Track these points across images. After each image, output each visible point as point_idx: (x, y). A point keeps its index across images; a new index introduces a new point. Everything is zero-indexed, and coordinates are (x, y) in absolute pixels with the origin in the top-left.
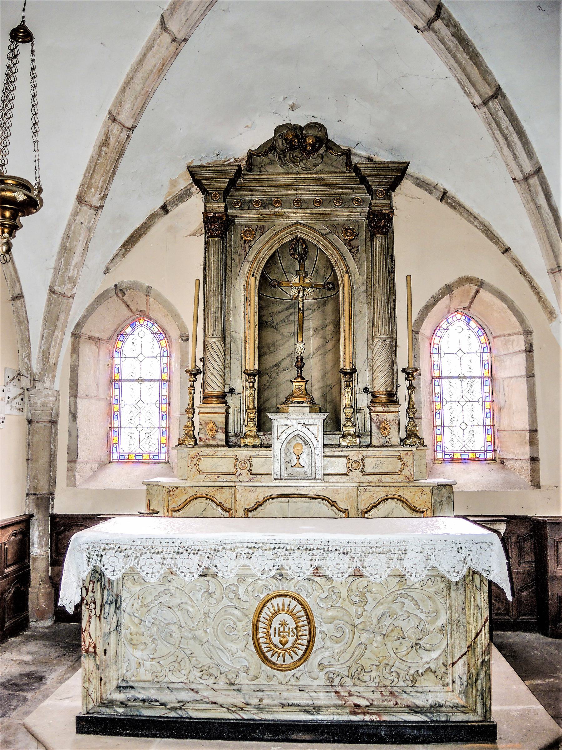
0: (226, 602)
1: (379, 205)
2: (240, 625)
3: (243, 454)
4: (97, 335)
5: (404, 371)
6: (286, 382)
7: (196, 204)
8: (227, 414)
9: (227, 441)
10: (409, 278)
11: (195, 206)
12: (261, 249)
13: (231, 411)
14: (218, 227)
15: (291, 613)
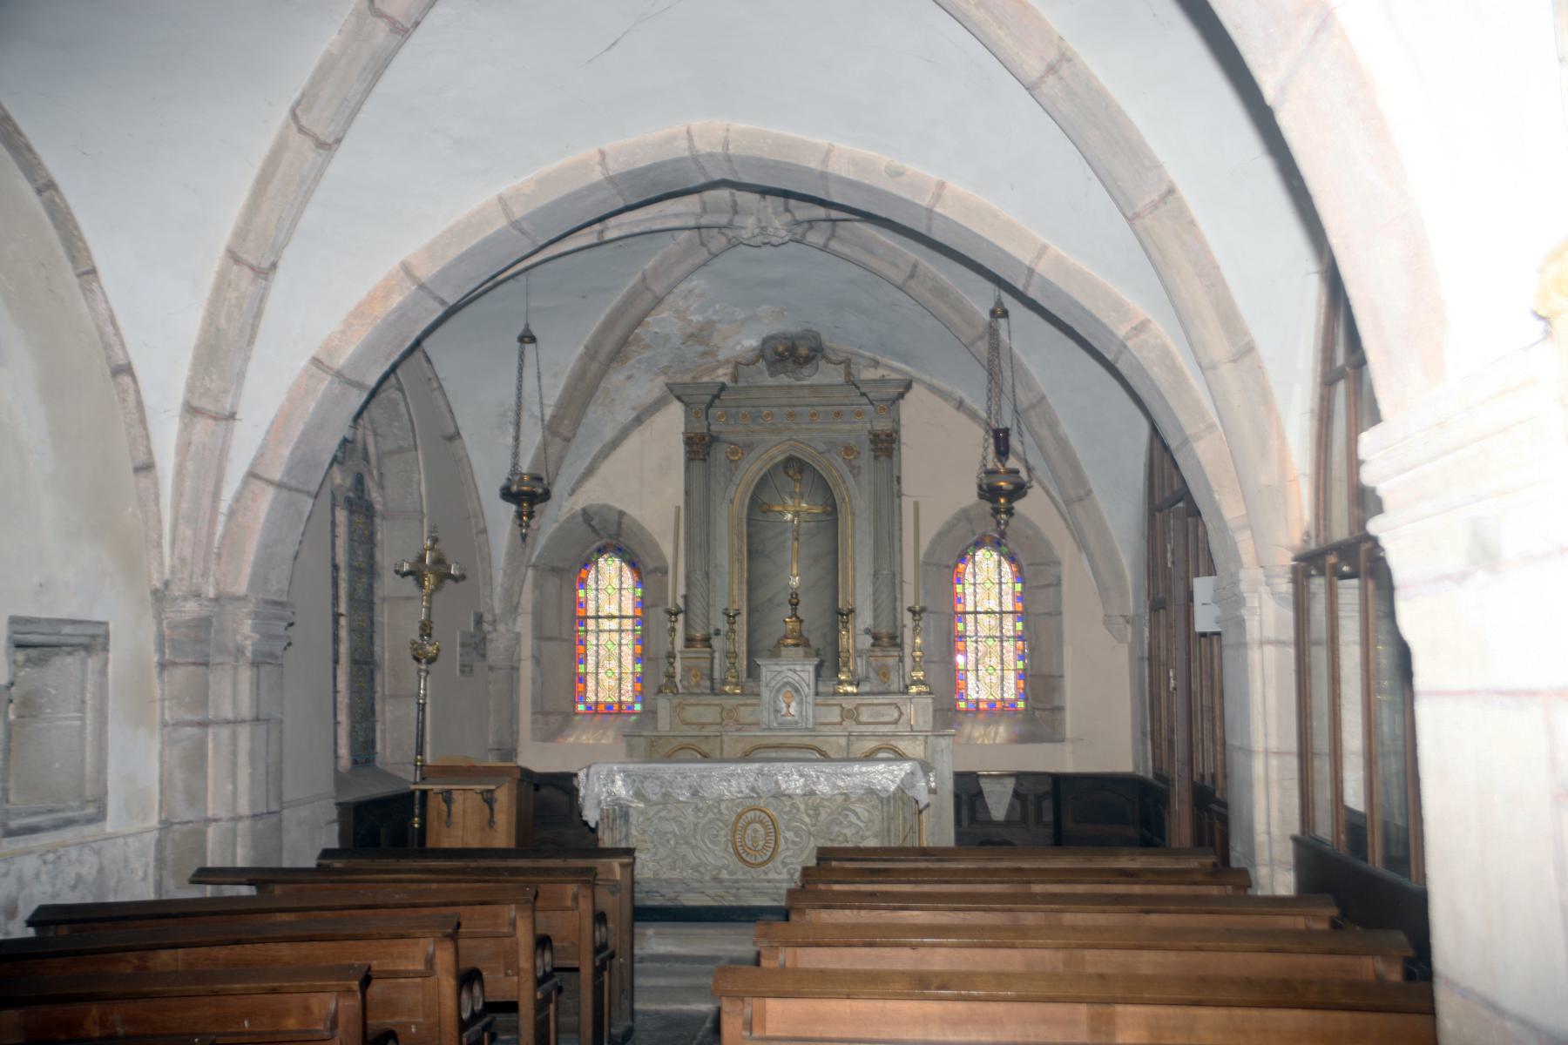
0: (711, 815)
1: (883, 425)
2: (723, 833)
3: (730, 702)
4: (560, 565)
5: (910, 609)
6: (781, 621)
7: (676, 411)
8: (712, 658)
9: (712, 689)
10: (916, 504)
11: (673, 419)
12: (752, 469)
13: (717, 655)
14: (699, 447)
15: (761, 822)
